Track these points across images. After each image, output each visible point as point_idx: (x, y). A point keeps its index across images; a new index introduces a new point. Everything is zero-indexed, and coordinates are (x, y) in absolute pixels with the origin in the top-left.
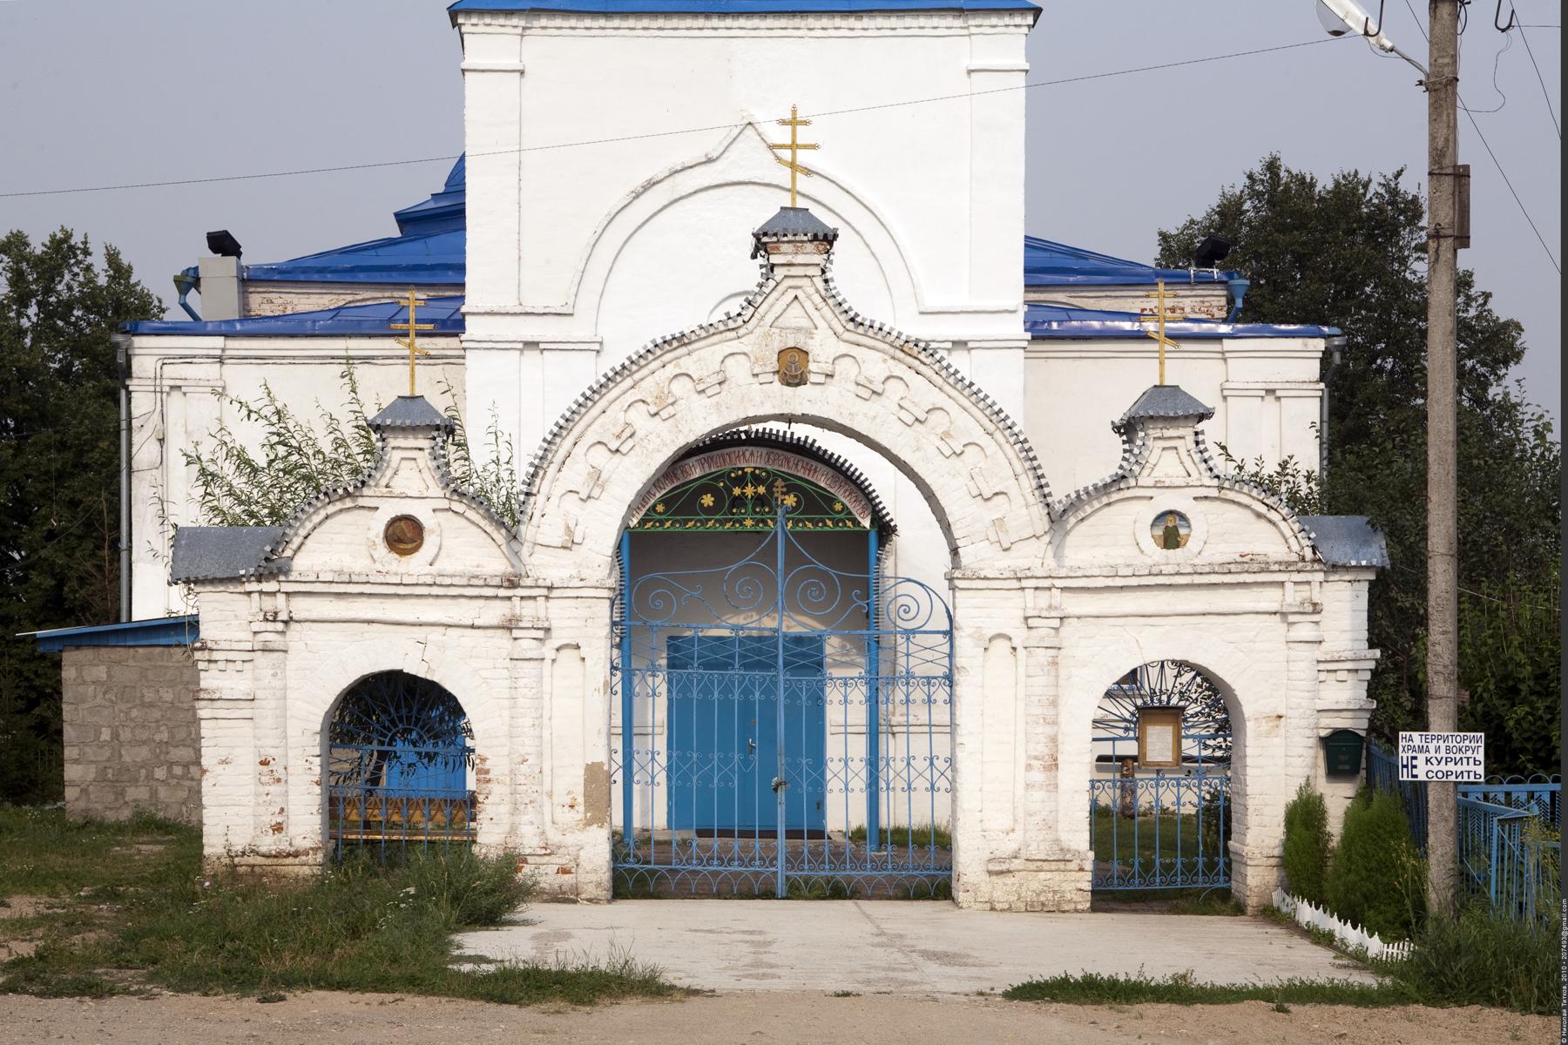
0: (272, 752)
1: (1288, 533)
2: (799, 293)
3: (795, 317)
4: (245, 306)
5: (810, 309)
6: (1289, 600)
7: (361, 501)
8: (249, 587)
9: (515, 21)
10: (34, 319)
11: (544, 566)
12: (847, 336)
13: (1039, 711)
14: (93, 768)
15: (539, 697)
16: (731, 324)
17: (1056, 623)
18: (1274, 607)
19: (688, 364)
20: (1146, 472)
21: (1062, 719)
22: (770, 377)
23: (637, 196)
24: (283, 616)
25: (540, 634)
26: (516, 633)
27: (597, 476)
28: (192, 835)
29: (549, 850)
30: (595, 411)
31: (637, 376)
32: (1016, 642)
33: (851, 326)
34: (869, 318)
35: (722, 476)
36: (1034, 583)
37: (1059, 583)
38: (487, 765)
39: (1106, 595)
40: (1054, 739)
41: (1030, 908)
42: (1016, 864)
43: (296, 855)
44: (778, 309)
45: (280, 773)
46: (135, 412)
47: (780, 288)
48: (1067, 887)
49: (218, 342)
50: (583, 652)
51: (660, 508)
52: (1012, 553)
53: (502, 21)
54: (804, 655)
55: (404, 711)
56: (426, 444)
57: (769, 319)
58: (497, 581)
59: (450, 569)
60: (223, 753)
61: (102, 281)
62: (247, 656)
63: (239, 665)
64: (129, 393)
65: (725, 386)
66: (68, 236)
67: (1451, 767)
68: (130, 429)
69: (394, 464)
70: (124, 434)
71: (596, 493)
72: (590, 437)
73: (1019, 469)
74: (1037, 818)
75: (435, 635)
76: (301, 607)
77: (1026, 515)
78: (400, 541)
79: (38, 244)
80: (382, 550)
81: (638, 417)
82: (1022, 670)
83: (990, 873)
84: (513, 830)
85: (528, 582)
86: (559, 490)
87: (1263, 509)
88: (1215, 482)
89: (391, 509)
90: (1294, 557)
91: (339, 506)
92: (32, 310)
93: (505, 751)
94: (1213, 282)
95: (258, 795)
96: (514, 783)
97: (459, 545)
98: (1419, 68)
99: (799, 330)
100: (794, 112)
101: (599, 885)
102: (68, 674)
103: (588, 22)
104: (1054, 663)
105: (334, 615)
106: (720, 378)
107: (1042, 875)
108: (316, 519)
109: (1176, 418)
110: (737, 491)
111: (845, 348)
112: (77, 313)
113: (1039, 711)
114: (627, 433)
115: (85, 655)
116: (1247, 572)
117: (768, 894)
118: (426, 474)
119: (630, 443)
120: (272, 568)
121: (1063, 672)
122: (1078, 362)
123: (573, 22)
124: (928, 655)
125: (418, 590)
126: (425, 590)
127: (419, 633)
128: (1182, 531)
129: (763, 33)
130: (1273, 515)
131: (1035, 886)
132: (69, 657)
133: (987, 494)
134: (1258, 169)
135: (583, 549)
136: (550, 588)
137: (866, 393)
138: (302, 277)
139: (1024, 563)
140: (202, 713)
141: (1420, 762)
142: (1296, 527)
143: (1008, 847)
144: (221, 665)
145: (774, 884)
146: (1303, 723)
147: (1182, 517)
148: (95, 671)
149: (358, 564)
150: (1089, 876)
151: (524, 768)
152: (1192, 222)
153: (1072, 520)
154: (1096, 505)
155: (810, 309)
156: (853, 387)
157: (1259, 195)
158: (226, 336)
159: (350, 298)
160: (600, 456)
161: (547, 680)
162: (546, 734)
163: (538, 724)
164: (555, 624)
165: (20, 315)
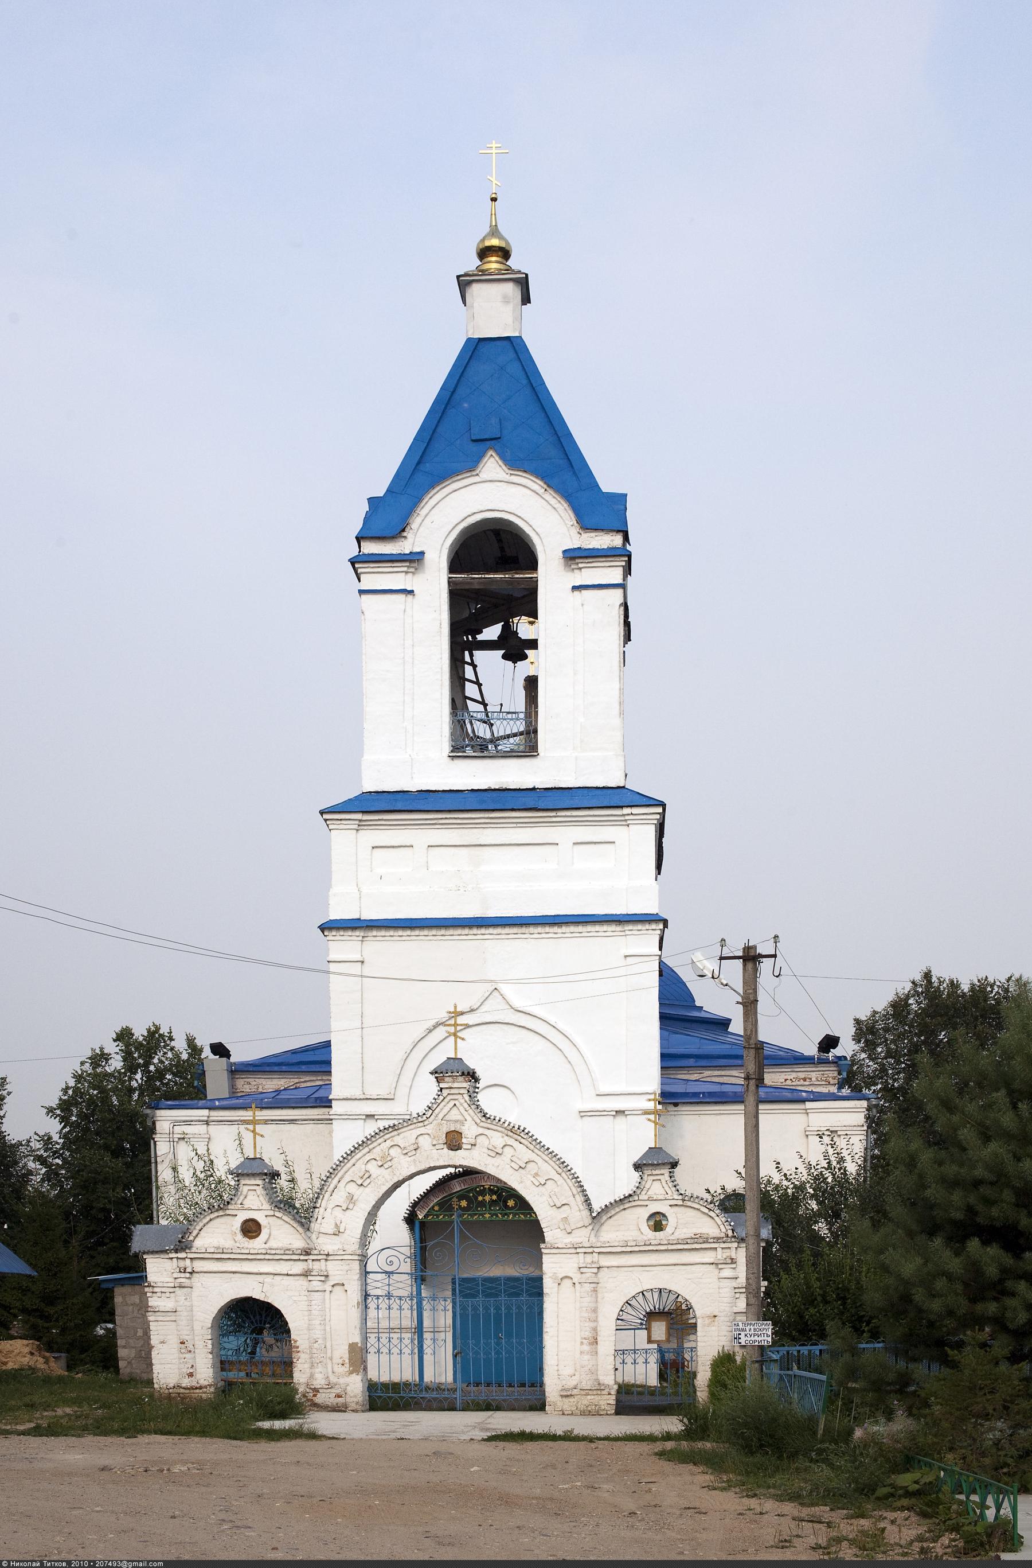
0: (187, 1337)
1: (720, 1223)
2: (456, 1102)
3: (454, 1115)
4: (233, 1087)
5: (463, 1111)
6: (719, 1257)
7: (228, 1212)
8: (171, 1255)
9: (357, 933)
10: (140, 1081)
11: (327, 1244)
12: (482, 1124)
13: (586, 1315)
14: (133, 1351)
15: (323, 1310)
16: (420, 1119)
17: (595, 1270)
18: (712, 1260)
19: (398, 1140)
20: (643, 1193)
21: (600, 1319)
22: (442, 1146)
23: (430, 1031)
24: (189, 1270)
25: (323, 1278)
26: (310, 1278)
27: (351, 1198)
28: (150, 1382)
29: (330, 1386)
30: (349, 1165)
31: (371, 1147)
32: (575, 1280)
33: (484, 1119)
34: (493, 1115)
35: (472, 1190)
36: (583, 1250)
37: (596, 1250)
38: (298, 1344)
39: (622, 1256)
40: (595, 1329)
41: (583, 1413)
42: (575, 1392)
43: (201, 1388)
44: (445, 1111)
45: (191, 1348)
46: (159, 1153)
47: (446, 1100)
48: (601, 1403)
49: (206, 1112)
50: (346, 1287)
51: (436, 1208)
52: (572, 1235)
53: (350, 933)
54: (471, 1289)
55: (258, 1317)
56: (260, 1182)
57: (441, 1116)
58: (299, 1252)
59: (275, 1246)
60: (162, 1338)
61: (185, 1056)
62: (172, 1290)
63: (168, 1295)
64: (155, 1143)
65: (418, 1151)
66: (158, 1028)
67: (756, 1338)
68: (156, 1162)
69: (244, 1193)
70: (153, 1165)
71: (351, 1206)
72: (347, 1178)
73: (575, 1192)
74: (586, 1369)
75: (268, 1279)
76: (199, 1265)
77: (578, 1214)
78: (249, 1232)
79: (140, 1032)
80: (240, 1236)
81: (372, 1167)
82: (578, 1294)
83: (562, 1396)
84: (312, 1376)
85: (316, 1252)
86: (331, 1205)
87: (706, 1211)
88: (680, 1197)
89: (243, 1216)
90: (723, 1235)
91: (216, 1214)
92: (138, 1076)
93: (306, 1337)
94: (829, 1063)
95: (180, 1359)
96: (311, 1353)
97: (280, 1233)
98: (739, 994)
99: (456, 1121)
100: (455, 1007)
101: (357, 1403)
102: (118, 1300)
103: (400, 933)
104: (595, 1291)
105: (215, 1269)
106: (415, 1146)
107: (589, 1397)
108: (205, 1221)
109: (658, 1165)
110: (480, 1198)
111: (481, 1131)
112: (169, 1077)
113: (586, 1315)
114: (367, 1175)
115: (127, 1289)
116: (699, 1242)
117: (452, 1408)
118: (261, 1198)
119: (368, 1181)
120: (182, 1245)
121: (600, 1295)
122: (718, 1117)
123: (391, 933)
124: (379, 1285)
125: (259, 1257)
126: (262, 1257)
127: (260, 1278)
128: (664, 1223)
129: (503, 937)
130: (711, 1214)
131: (586, 1402)
132: (118, 1290)
133: (559, 1205)
134: (918, 977)
135: (345, 1235)
136: (328, 1255)
137: (493, 1154)
138: (268, 1069)
139: (579, 1240)
140: (150, 1318)
141: (742, 1336)
142: (724, 1219)
143: (572, 1383)
144: (159, 1294)
145: (455, 1404)
146: (727, 1319)
147: (664, 1215)
148: (132, 1298)
149: (227, 1243)
150: (614, 1397)
151: (316, 1345)
152: (875, 1012)
153: (605, 1218)
154: (617, 1210)
155: (463, 1111)
156: (486, 1150)
157: (918, 994)
158: (210, 1109)
159: (297, 1081)
160: (352, 1188)
161: (327, 1301)
162: (328, 1328)
163: (323, 1323)
164: (330, 1273)
165: (131, 1079)
